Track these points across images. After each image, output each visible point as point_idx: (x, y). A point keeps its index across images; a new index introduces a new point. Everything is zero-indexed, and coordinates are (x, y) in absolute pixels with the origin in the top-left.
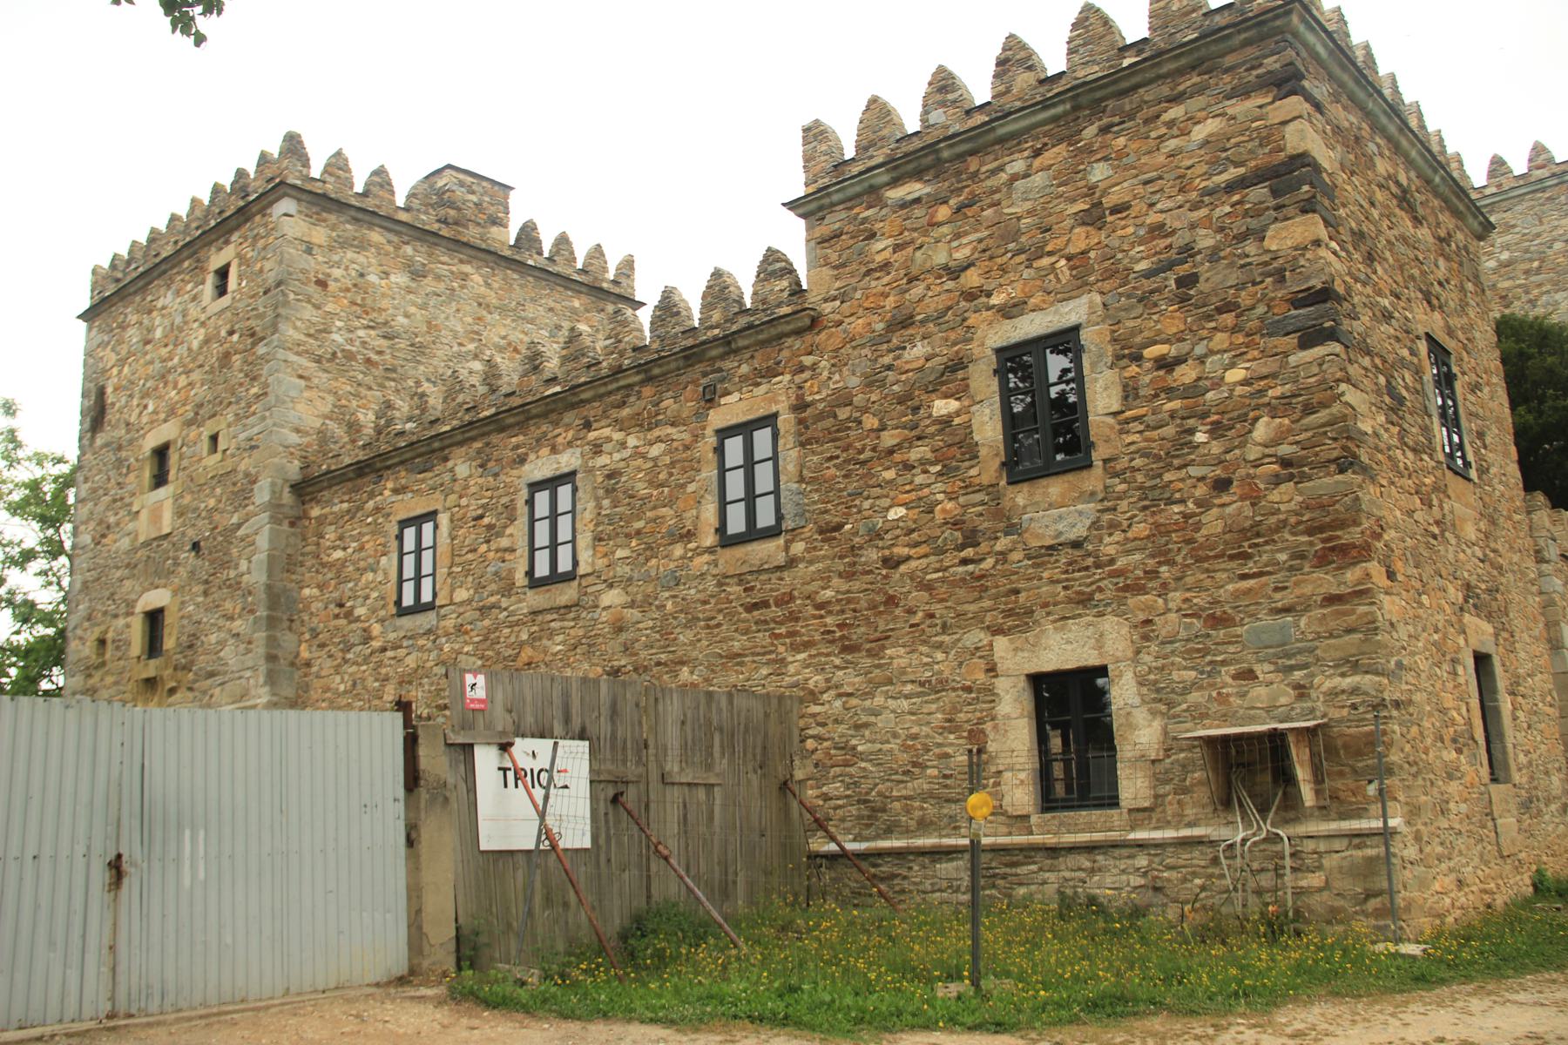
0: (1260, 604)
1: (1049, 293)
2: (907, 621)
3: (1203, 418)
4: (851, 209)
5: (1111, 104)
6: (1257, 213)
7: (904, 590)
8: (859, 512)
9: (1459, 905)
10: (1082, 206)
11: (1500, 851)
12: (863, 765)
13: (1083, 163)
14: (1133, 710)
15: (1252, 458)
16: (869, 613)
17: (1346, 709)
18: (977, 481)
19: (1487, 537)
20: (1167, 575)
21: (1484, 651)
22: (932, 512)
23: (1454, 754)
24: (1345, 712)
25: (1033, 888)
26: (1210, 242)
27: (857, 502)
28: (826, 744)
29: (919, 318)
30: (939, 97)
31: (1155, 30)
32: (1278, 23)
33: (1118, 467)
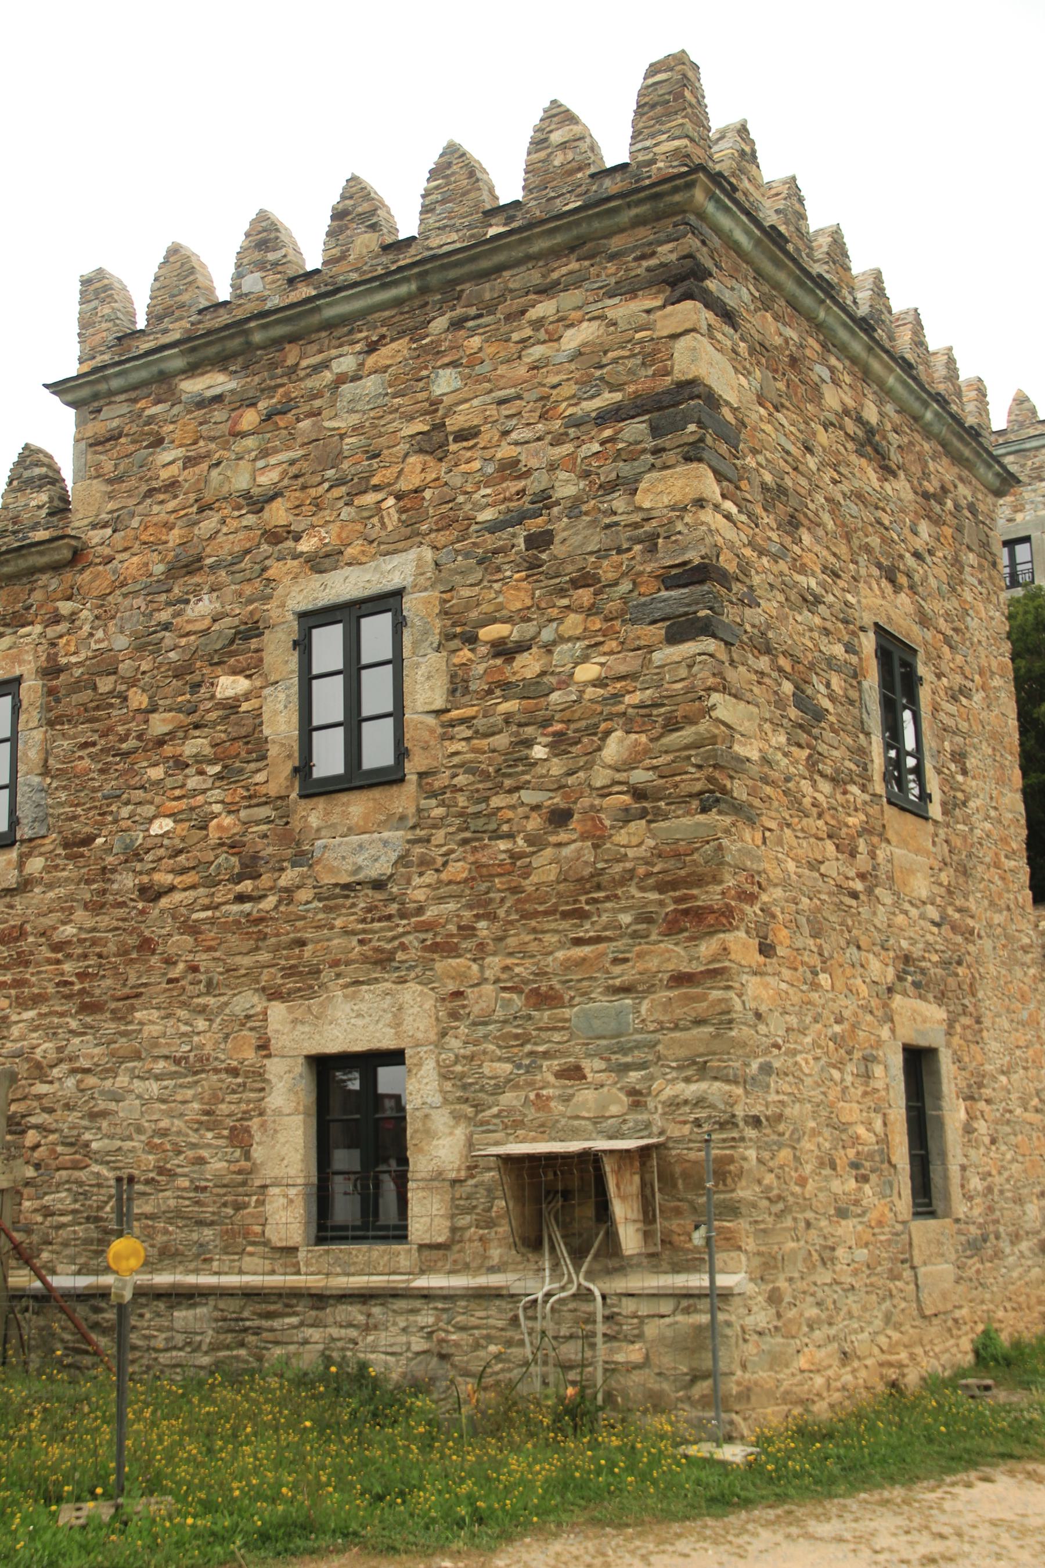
0: (595, 979)
1: (372, 542)
2: (165, 974)
3: (545, 727)
4: (135, 401)
5: (468, 288)
6: (630, 455)
7: (164, 932)
8: (116, 821)
9: (839, 1384)
10: (420, 426)
11: (920, 1309)
12: (96, 1168)
13: (426, 368)
14: (432, 1112)
15: (598, 784)
16: (118, 960)
17: (688, 1126)
18: (263, 790)
19: (950, 893)
20: (485, 933)
21: (923, 1043)
22: (205, 828)
23: (852, 1184)
24: (686, 1129)
25: (292, 1348)
26: (570, 490)
27: (114, 808)
28: (52, 1137)
29: (209, 561)
30: (257, 256)
31: (531, 191)
32: (677, 198)
33: (437, 785)
